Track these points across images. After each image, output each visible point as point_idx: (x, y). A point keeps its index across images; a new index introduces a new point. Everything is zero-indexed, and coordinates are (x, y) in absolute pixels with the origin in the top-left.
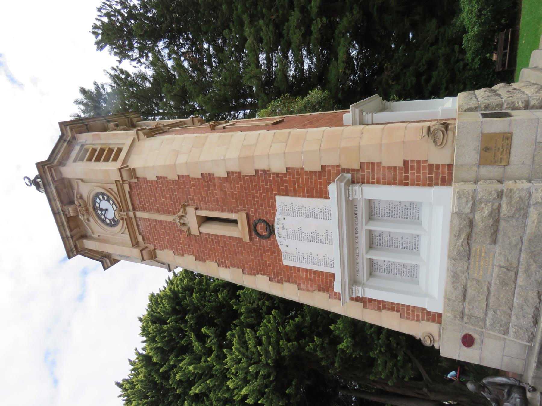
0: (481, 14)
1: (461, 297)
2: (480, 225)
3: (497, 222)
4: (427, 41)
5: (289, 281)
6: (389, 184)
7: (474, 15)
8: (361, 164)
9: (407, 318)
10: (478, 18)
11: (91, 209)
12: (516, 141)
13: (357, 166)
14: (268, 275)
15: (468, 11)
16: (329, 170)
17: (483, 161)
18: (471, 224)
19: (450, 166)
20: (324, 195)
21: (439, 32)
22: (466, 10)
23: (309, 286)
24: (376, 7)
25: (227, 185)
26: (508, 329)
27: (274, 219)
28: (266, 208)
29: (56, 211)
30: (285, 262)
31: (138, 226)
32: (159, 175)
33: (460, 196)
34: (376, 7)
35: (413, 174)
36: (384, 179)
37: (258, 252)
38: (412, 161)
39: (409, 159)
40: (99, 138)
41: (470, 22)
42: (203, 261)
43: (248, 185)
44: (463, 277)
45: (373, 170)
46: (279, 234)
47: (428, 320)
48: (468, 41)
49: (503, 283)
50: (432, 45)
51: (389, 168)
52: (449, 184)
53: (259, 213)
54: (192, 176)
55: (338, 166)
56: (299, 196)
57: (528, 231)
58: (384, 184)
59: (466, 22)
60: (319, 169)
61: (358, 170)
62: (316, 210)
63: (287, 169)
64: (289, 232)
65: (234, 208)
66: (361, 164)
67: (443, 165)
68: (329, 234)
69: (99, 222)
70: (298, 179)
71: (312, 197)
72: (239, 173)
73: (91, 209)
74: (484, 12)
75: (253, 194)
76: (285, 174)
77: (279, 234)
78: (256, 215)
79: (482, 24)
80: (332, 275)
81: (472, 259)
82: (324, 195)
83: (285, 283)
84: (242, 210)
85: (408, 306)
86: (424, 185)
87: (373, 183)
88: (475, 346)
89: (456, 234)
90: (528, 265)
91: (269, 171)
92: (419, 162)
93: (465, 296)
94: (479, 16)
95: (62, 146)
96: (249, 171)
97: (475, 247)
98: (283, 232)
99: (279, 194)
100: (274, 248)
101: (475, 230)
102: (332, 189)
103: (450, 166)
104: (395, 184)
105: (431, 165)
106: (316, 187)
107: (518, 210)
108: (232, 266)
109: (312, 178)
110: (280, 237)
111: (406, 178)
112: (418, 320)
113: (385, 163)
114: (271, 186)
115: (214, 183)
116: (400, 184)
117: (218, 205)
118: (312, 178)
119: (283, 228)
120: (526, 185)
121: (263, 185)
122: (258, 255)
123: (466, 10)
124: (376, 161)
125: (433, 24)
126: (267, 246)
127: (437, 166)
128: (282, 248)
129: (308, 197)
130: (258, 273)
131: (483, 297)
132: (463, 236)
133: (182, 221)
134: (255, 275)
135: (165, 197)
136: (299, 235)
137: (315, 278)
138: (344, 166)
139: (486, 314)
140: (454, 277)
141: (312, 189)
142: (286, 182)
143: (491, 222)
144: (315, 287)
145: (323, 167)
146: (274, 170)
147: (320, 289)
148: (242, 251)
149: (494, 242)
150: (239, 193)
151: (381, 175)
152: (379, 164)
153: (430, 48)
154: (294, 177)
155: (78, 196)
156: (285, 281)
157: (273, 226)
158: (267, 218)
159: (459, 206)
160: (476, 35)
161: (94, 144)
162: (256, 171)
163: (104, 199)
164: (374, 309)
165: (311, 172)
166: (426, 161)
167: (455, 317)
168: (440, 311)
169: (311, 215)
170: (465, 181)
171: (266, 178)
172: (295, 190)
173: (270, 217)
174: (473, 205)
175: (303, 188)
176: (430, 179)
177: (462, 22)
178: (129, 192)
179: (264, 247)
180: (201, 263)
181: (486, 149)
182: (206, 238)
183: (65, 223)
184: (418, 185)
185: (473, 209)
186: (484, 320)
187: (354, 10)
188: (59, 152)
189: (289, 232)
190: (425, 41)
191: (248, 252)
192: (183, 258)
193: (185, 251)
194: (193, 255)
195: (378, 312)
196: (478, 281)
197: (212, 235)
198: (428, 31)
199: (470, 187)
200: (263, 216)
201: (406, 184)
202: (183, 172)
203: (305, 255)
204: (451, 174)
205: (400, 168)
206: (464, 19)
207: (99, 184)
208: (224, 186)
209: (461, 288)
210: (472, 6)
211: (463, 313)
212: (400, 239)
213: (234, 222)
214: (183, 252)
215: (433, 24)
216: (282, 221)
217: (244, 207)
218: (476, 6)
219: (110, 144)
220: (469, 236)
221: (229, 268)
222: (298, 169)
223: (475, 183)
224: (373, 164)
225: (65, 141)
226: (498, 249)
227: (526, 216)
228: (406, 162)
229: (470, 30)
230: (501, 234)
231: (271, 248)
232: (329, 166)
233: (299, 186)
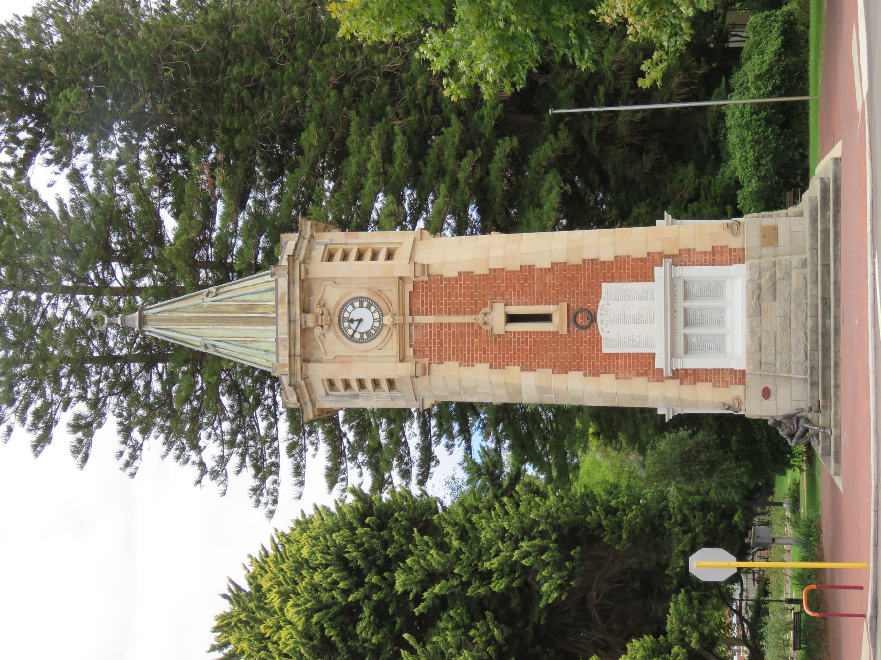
0: (759, 165)
1: (757, 347)
2: (765, 287)
3: (775, 283)
4: (682, 196)
5: (606, 373)
6: (702, 265)
7: (750, 164)
8: (680, 250)
9: (719, 387)
10: (756, 170)
12: (781, 231)
13: (676, 252)
15: (741, 158)
17: (763, 245)
18: (759, 287)
19: (743, 249)
20: (650, 278)
21: (700, 184)
22: (738, 156)
24: (594, 133)
25: (548, 277)
27: (597, 307)
29: (292, 319)
30: (605, 350)
31: (411, 335)
32: (463, 270)
34: (594, 133)
36: (697, 261)
37: (574, 345)
40: (357, 238)
41: (746, 173)
45: (689, 255)
46: (601, 320)
47: (735, 384)
48: (745, 199)
49: (784, 330)
50: (690, 201)
51: (701, 253)
52: (744, 263)
54: (508, 269)
55: (661, 253)
56: (625, 281)
57: (793, 287)
58: (698, 265)
59: (740, 174)
60: (644, 255)
61: (676, 256)
66: (680, 250)
69: (343, 338)
70: (625, 266)
71: (637, 281)
72: (565, 263)
74: (763, 162)
76: (612, 262)
77: (601, 320)
78: (577, 304)
79: (761, 179)
80: (653, 355)
81: (763, 315)
82: (650, 278)
83: (602, 376)
85: (719, 370)
86: (727, 265)
87: (689, 265)
90: (796, 312)
92: (722, 247)
93: (760, 347)
94: (757, 165)
95: (302, 243)
96: (576, 260)
97: (764, 304)
99: (605, 281)
100: (593, 337)
101: (763, 291)
102: (659, 271)
103: (743, 249)
104: (706, 265)
105: (730, 249)
107: (786, 273)
108: (539, 367)
109: (637, 264)
110: (602, 323)
111: (714, 260)
112: (727, 387)
113: (698, 250)
115: (534, 276)
116: (710, 265)
117: (534, 298)
118: (637, 264)
119: (606, 314)
120: (788, 257)
123: (738, 156)
124: (691, 247)
125: (689, 171)
127: (735, 250)
128: (601, 334)
131: (772, 344)
132: (755, 297)
133: (486, 319)
134: (566, 373)
138: (666, 253)
140: (752, 332)
141: (637, 274)
142: (613, 268)
143: (771, 283)
145: (649, 254)
146: (602, 259)
147: (639, 374)
149: (775, 299)
150: (561, 284)
151: (695, 258)
152: (694, 250)
153: (689, 205)
154: (621, 264)
157: (595, 314)
159: (751, 275)
160: (755, 193)
161: (345, 244)
162: (584, 260)
163: (361, 306)
165: (637, 259)
166: (727, 247)
168: (743, 367)
170: (753, 258)
174: (760, 273)
176: (731, 260)
177: (734, 172)
179: (582, 338)
181: (764, 236)
182: (511, 339)
183: (298, 336)
184: (722, 265)
185: (760, 277)
187: (560, 132)
188: (301, 249)
190: (678, 196)
194: (488, 362)
195: (694, 386)
196: (768, 332)
197: (519, 333)
198: (682, 181)
199: (757, 261)
200: (585, 304)
201: (714, 265)
202: (498, 265)
203: (627, 339)
204: (744, 255)
205: (710, 253)
206: (736, 168)
208: (545, 278)
210: (746, 152)
213: (547, 318)
214: (473, 362)
215: (689, 171)
217: (565, 297)
218: (752, 153)
219: (375, 244)
220: (759, 296)
221: (535, 370)
223: (760, 258)
224: (689, 250)
225: (304, 238)
226: (777, 303)
227: (790, 277)
228: (713, 248)
229: (745, 184)
230: (778, 291)
233: (625, 272)
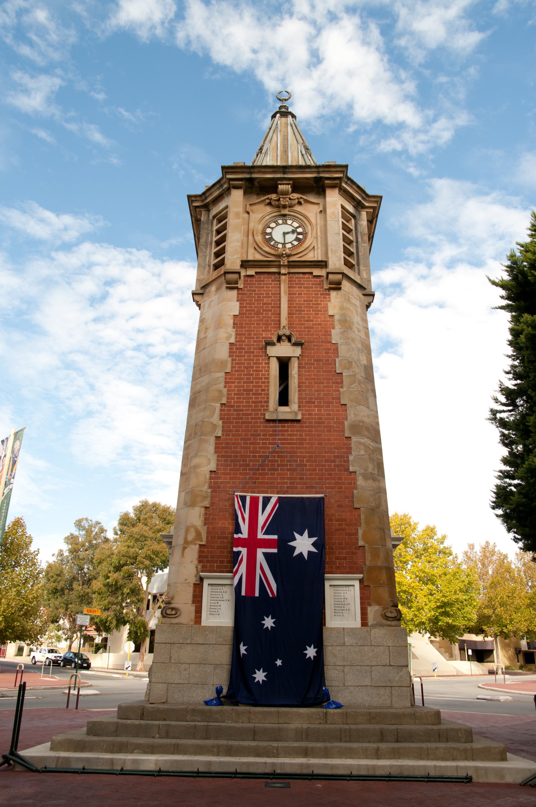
194: (236, 341)
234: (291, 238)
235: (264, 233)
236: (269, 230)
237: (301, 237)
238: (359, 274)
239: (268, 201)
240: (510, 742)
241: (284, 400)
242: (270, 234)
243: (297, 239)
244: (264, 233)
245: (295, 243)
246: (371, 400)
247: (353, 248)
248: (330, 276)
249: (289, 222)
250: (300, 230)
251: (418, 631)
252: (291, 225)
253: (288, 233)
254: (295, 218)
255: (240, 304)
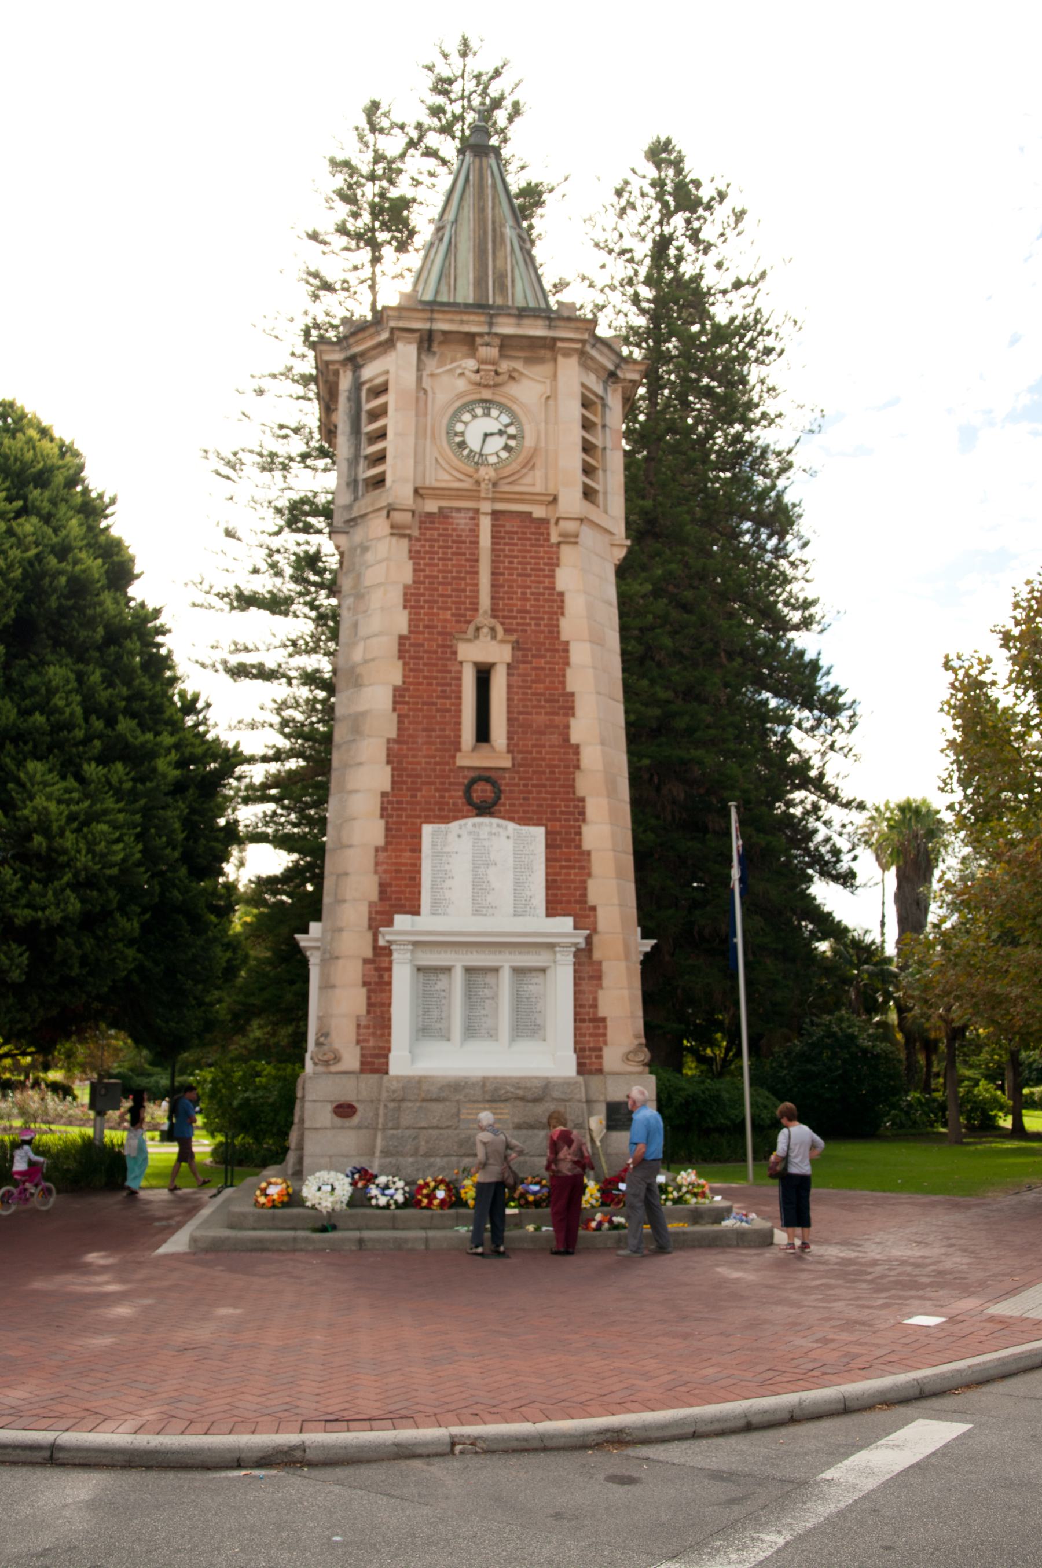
8: (600, 963)
11: (487, 394)
13: (597, 955)
14: (393, 788)
16: (588, 916)
19: (600, 1071)
20: (551, 911)
23: (385, 867)
25: (555, 739)
26: (392, 1155)
28: (521, 805)
33: (567, 1083)
35: (588, 1028)
37: (436, 777)
38: (605, 1027)
39: (609, 1023)
42: (400, 651)
43: (558, 779)
44: (460, 1097)
45: (591, 978)
46: (480, 824)
51: (595, 999)
53: (511, 792)
54: (569, 672)
61: (590, 957)
62: (529, 893)
63: (589, 853)
64: (486, 843)
65: (517, 745)
67: (601, 1064)
68: (490, 911)
70: (573, 867)
71: (548, 888)
72: (578, 767)
73: (487, 394)
75: (544, 786)
76: (579, 846)
77: (480, 824)
82: (551, 911)
83: (382, 822)
84: (513, 759)
86: (576, 1043)
88: (338, 1121)
89: (519, 1083)
91: (584, 820)
92: (604, 1035)
98: (484, 833)
105: (600, 1049)
106: (563, 895)
109: (576, 889)
110: (474, 825)
111: (583, 1021)
112: (358, 1042)
113: (601, 994)
114: (559, 820)
121: (559, 806)
122: (429, 776)
126: (451, 797)
127: (600, 1057)
128: (455, 826)
129: (547, 881)
130: (393, 769)
131: (435, 1122)
132: (520, 1093)
135: (524, 599)
136: (481, 861)
137: (403, 879)
139: (407, 1128)
141: (559, 888)
144: (387, 877)
145: (594, 909)
146: (585, 829)
147: (383, 888)
148: (434, 743)
155: (515, 374)
156: (387, 823)
158: (504, 805)
164: (364, 975)
165: (585, 889)
167: (394, 1092)
169: (518, 884)
170: (587, 1086)
171: (573, 813)
172: (556, 860)
173: (506, 811)
175: (559, 874)
178: (530, 513)
180: (395, 647)
182: (450, 672)
186: (397, 1128)
189: (486, 843)
191: (434, 757)
192: (401, 607)
193: (418, 614)
194: (410, 632)
195: (360, 981)
200: (508, 798)
201: (575, 1021)
203: (447, 867)
204: (590, 1073)
205: (595, 1013)
207: (543, 437)
209: (443, 1095)
211: (403, 1100)
212: (483, 1012)
216: (503, 834)
220: (522, 1099)
221: (394, 710)
222: (589, 868)
231: (448, 804)
232: (595, 916)
234: (496, 444)
235: (451, 433)
236: (459, 427)
237: (512, 443)
238: (606, 512)
239: (459, 371)
240: (909, 1362)
241: (483, 734)
242: (462, 434)
243: (507, 448)
244: (451, 433)
245: (504, 455)
246: (664, 1096)
247: (595, 415)
248: (562, 523)
249: (494, 412)
250: (512, 430)
251: (882, 808)
252: (497, 419)
253: (492, 434)
254: (503, 408)
255: (415, 564)
